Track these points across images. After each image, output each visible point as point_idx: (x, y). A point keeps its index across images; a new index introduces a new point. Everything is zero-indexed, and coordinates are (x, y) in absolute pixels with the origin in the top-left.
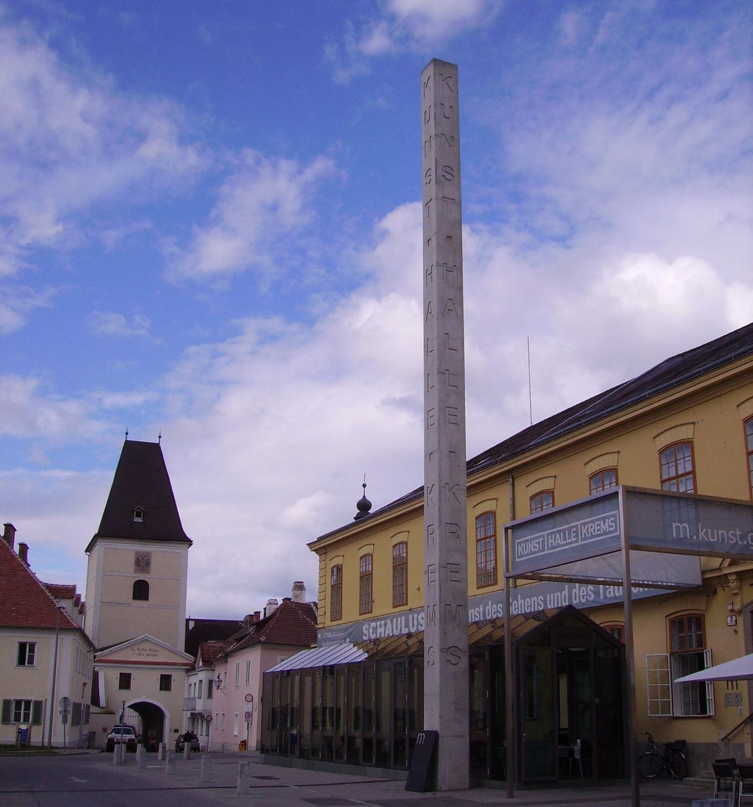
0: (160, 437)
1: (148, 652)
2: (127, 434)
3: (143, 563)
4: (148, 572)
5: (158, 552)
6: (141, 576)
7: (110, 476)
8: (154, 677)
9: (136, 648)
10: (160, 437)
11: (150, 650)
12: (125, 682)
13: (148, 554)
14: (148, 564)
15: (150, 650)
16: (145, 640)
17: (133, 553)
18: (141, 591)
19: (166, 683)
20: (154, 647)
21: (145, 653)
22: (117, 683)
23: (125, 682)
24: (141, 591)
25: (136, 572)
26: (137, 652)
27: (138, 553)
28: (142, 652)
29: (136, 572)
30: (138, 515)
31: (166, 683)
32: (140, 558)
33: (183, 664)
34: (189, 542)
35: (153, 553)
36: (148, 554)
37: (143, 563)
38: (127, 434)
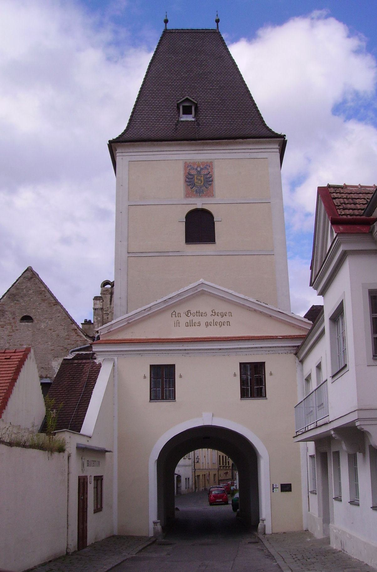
0: (217, 21)
1: (210, 319)
2: (166, 21)
3: (199, 180)
4: (211, 194)
5: (228, 163)
6: (199, 203)
7: (307, 311)
8: (225, 375)
9: (182, 310)
10: (217, 21)
11: (214, 313)
12: (163, 382)
13: (209, 165)
14: (208, 181)
15: (214, 313)
16: (200, 293)
17: (181, 166)
18: (200, 227)
19: (253, 381)
20: (222, 308)
21: (203, 320)
22: (143, 386)
23: (163, 382)
24: (200, 227)
25: (187, 195)
26: (184, 319)
27: (188, 166)
28: (196, 319)
29: (187, 195)
30: (187, 111)
31: (253, 381)
32: (193, 172)
33: (284, 338)
34: (281, 142)
35: (216, 163)
36: (209, 165)
37: (199, 180)
38: (166, 21)
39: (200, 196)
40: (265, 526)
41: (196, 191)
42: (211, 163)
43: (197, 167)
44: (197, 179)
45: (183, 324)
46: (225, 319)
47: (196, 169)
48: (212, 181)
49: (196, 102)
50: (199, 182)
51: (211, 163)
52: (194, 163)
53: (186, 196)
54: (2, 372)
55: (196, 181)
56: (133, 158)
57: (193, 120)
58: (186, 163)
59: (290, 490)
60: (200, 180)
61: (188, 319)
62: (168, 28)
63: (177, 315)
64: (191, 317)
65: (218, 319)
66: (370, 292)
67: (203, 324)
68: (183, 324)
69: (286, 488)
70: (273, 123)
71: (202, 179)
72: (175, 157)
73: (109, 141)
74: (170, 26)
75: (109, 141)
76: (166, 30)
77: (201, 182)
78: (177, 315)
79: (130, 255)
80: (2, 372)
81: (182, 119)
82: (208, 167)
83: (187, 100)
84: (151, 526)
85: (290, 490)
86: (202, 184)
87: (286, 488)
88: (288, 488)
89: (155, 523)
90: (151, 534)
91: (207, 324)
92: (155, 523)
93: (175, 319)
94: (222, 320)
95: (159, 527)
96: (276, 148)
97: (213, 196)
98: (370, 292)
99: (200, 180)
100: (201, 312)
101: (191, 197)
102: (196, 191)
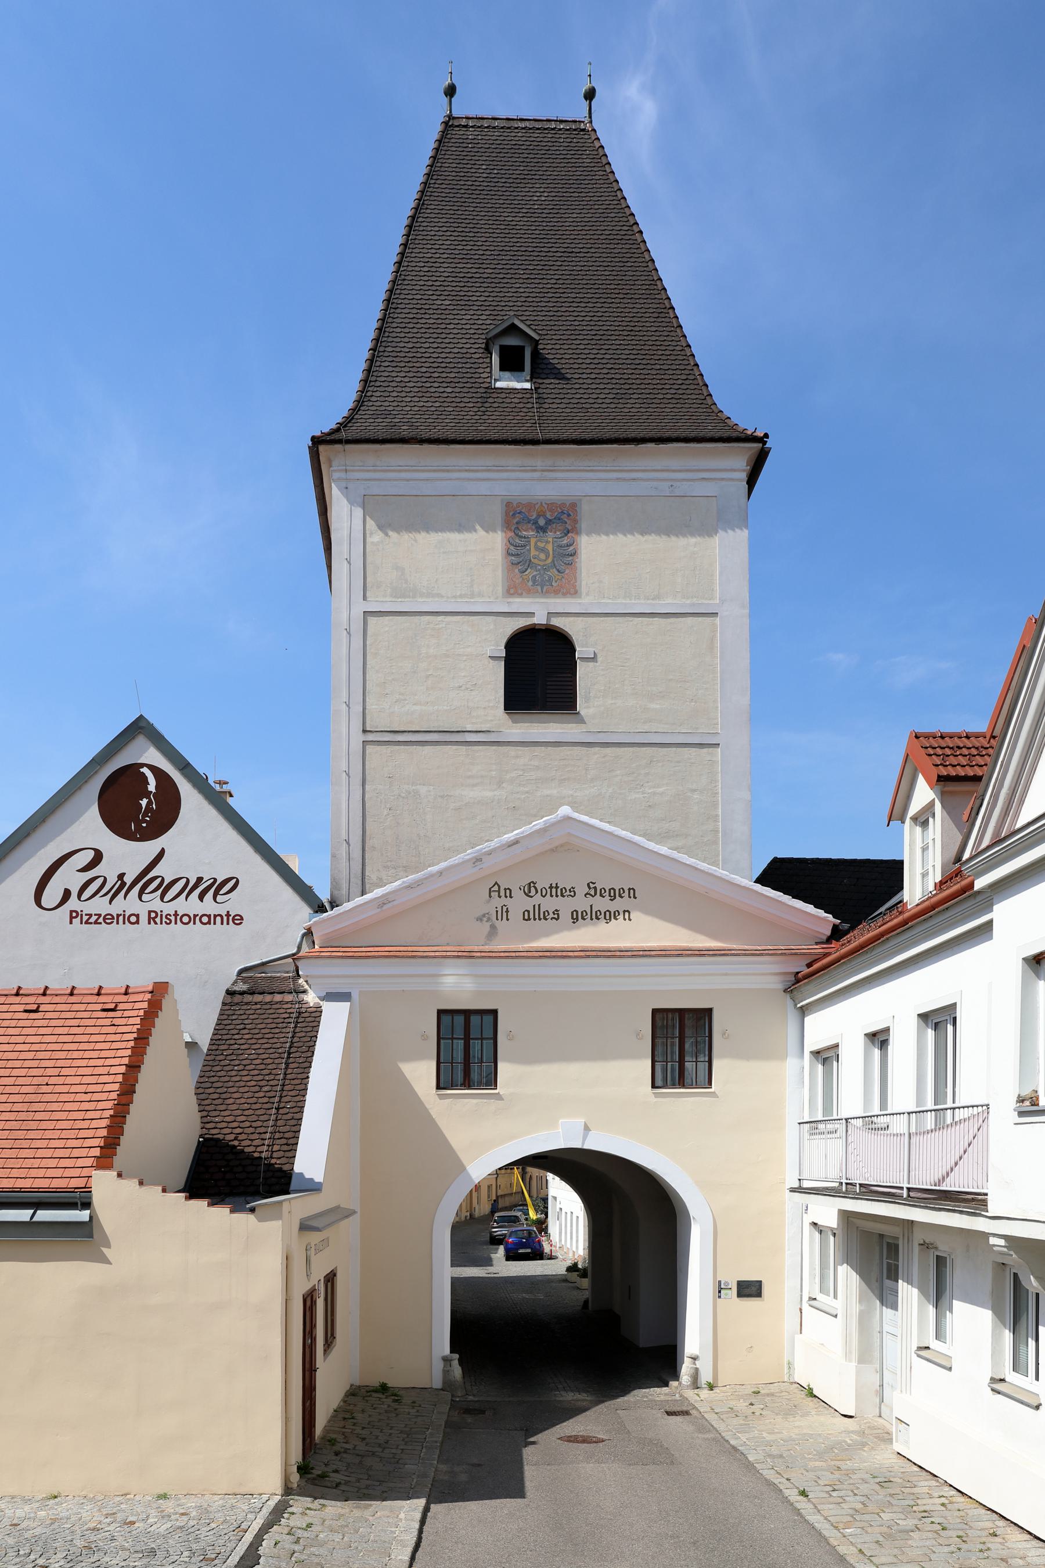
0: (590, 95)
1: (581, 903)
2: (451, 91)
4: (572, 590)
6: (539, 610)
15: (593, 890)
18: (540, 671)
21: (566, 906)
25: (512, 590)
26: (519, 903)
28: (549, 904)
29: (512, 590)
30: (511, 362)
39: (545, 594)
40: (697, 1370)
41: (534, 578)
42: (574, 506)
43: (539, 516)
44: (537, 548)
45: (516, 914)
46: (618, 904)
47: (536, 523)
48: (574, 554)
49: (537, 337)
50: (542, 556)
51: (574, 506)
52: (530, 506)
53: (508, 591)
54: (6, 1023)
55: (533, 552)
56: (376, 489)
57: (527, 385)
58: (508, 504)
59: (758, 1294)
60: (543, 550)
61: (528, 904)
62: (455, 114)
63: (502, 893)
64: (537, 899)
65: (602, 904)
66: (232, 1212)
67: (565, 916)
68: (516, 914)
69: (749, 1290)
70: (735, 402)
71: (550, 547)
72: (484, 488)
73: (313, 438)
74: (463, 107)
75: (313, 438)
76: (450, 117)
77: (547, 557)
78: (502, 893)
79: (370, 737)
80: (6, 1023)
81: (499, 384)
82: (564, 517)
83: (513, 329)
84: (438, 1366)
85: (758, 1294)
86: (550, 560)
87: (749, 1290)
88: (754, 1289)
89: (445, 1359)
90: (437, 1383)
91: (576, 917)
92: (445, 1359)
93: (498, 902)
94: (613, 906)
95: (457, 1371)
96: (735, 462)
97: (576, 592)
98: (232, 1212)
99: (543, 550)
100: (561, 886)
101: (520, 595)
102: (534, 581)
